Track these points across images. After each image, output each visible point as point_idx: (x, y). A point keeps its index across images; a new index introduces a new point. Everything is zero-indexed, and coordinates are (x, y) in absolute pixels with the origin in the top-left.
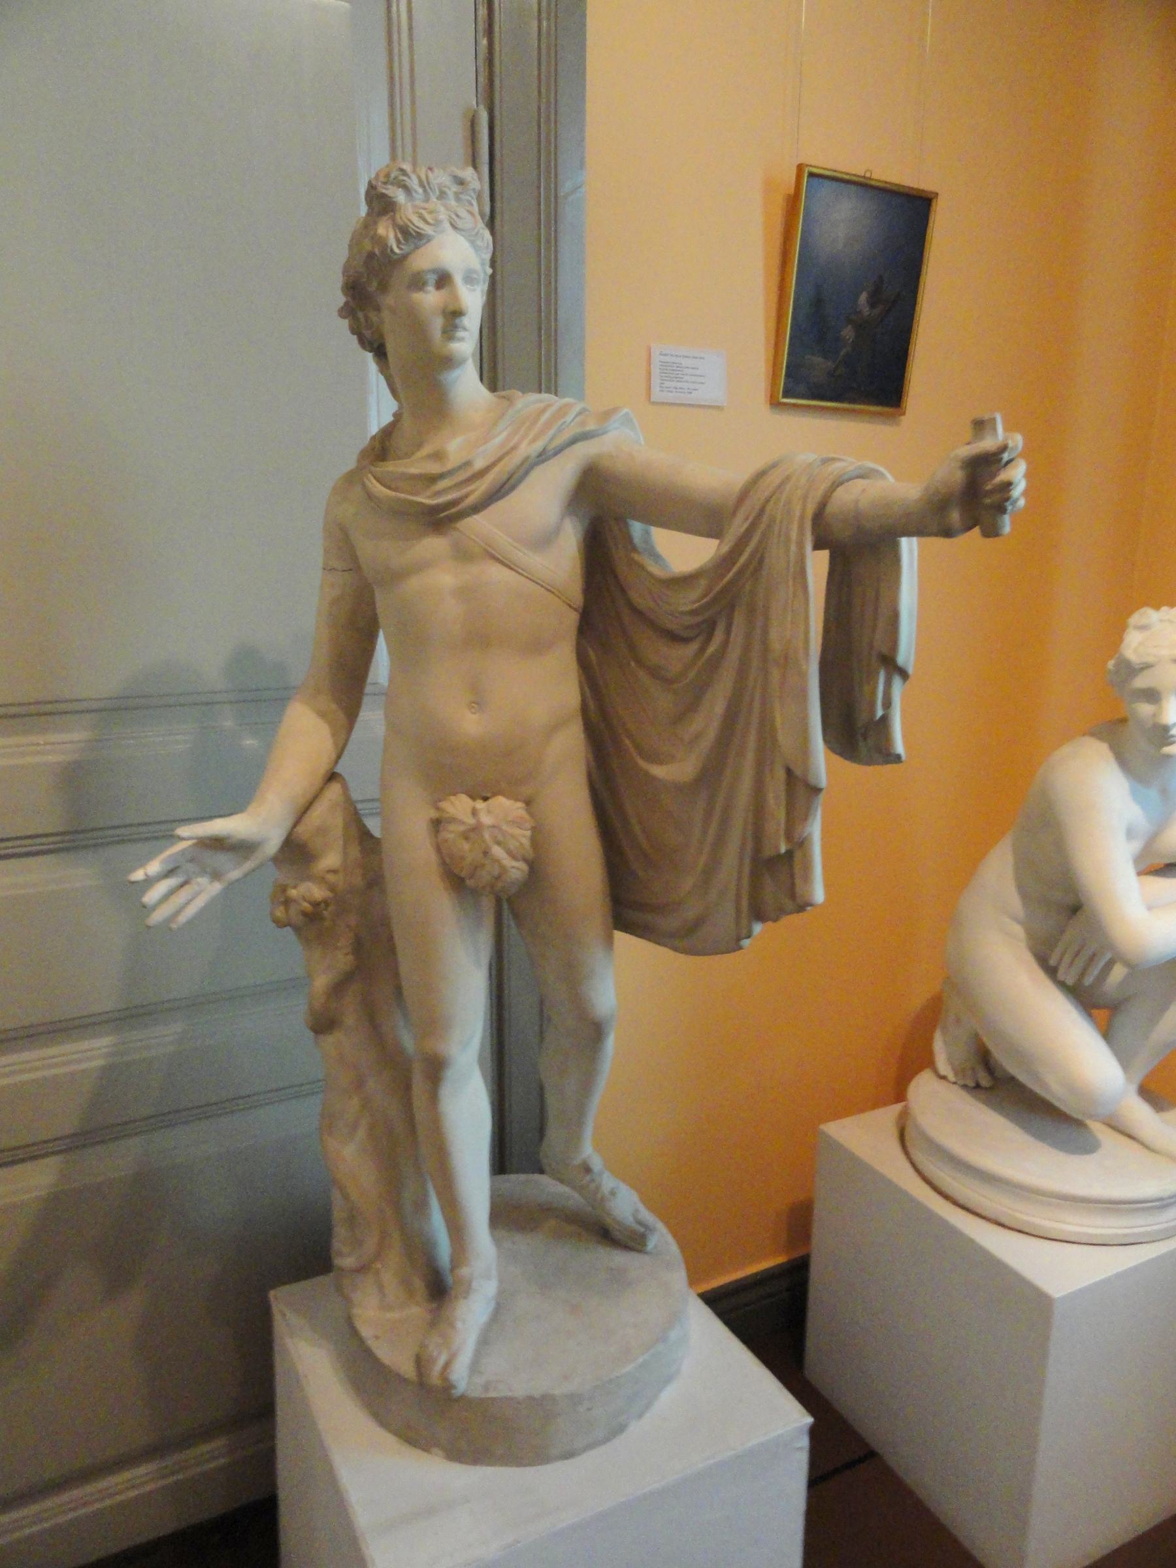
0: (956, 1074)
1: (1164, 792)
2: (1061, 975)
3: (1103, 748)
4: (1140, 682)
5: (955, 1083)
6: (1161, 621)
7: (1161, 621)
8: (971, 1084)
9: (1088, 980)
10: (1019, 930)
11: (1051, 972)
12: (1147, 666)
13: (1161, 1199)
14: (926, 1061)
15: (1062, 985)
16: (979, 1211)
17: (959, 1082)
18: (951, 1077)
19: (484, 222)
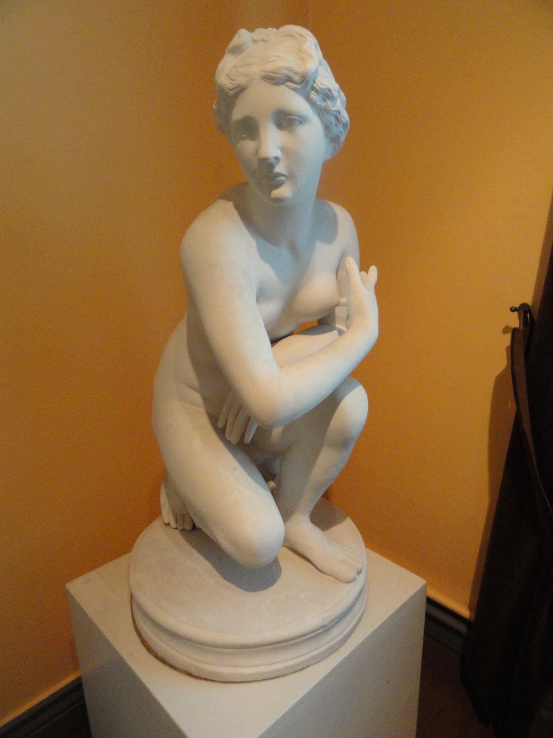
0: (176, 522)
1: (293, 249)
2: (227, 436)
3: (230, 205)
4: (237, 114)
5: (176, 528)
6: (254, 41)
7: (254, 41)
8: (188, 527)
9: (248, 439)
10: (197, 397)
11: (221, 432)
12: (241, 90)
13: (324, 626)
14: (156, 513)
15: (227, 443)
16: (172, 662)
17: (178, 528)
18: (173, 524)
19: (368, 289)
